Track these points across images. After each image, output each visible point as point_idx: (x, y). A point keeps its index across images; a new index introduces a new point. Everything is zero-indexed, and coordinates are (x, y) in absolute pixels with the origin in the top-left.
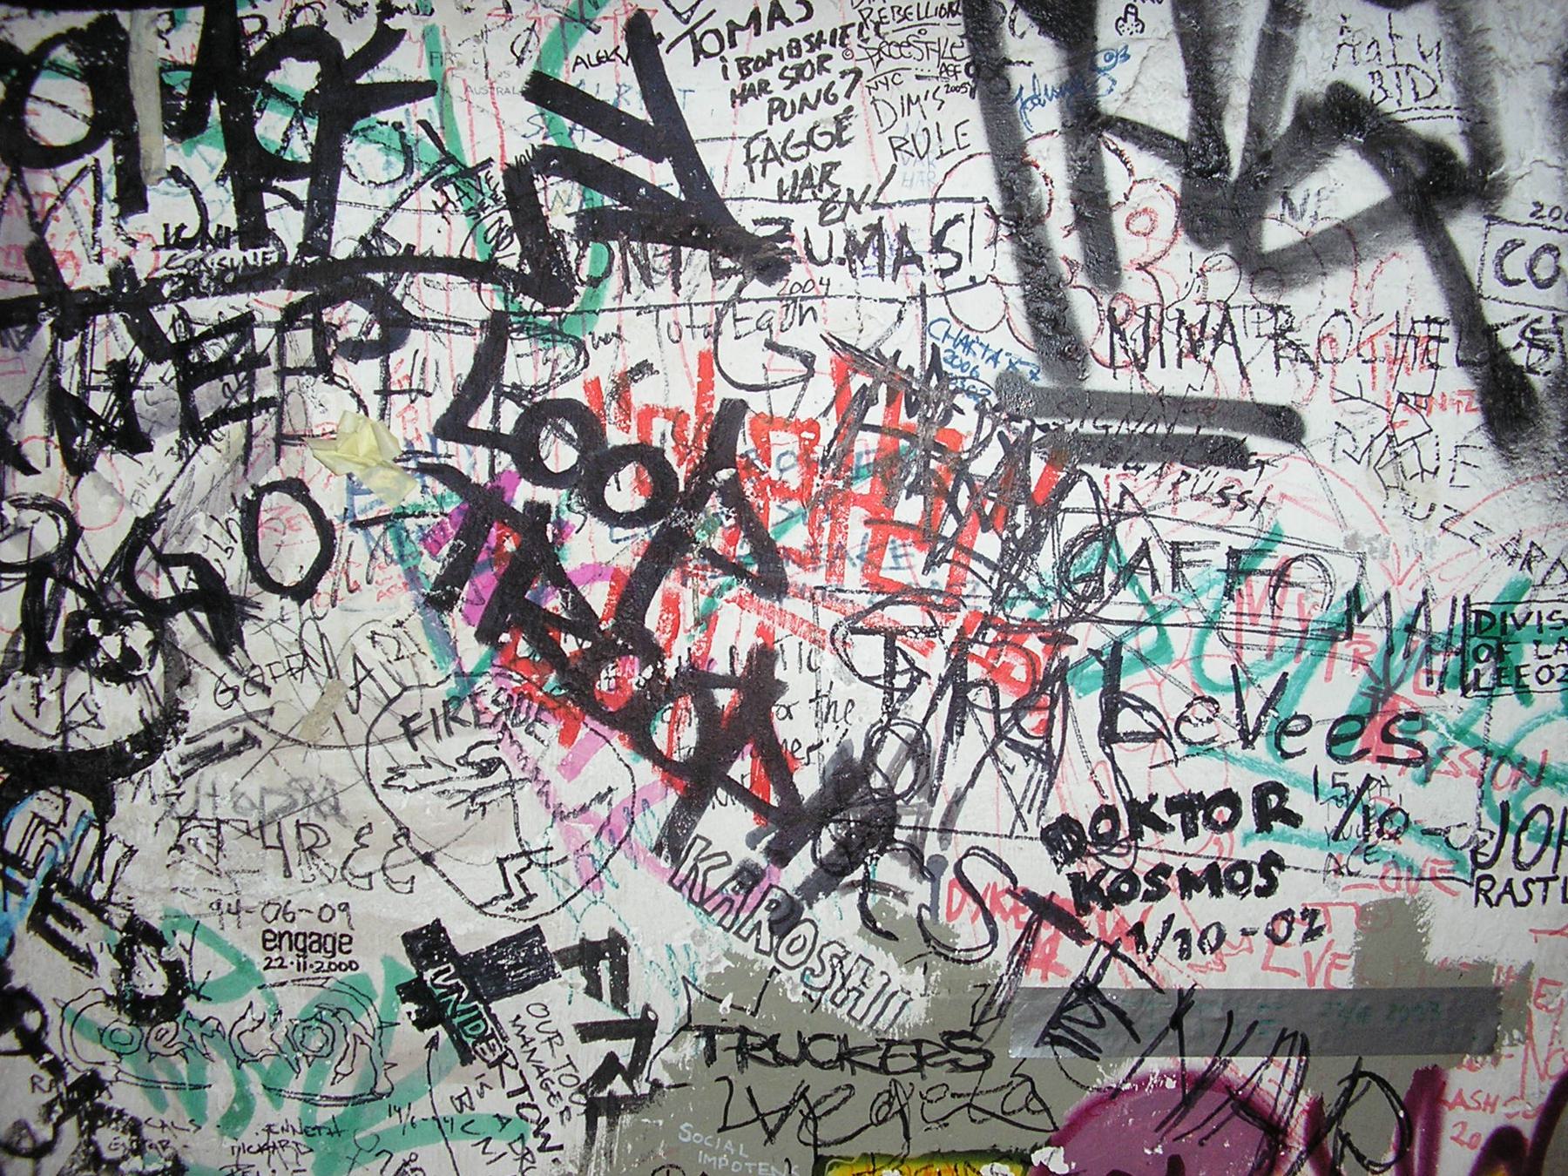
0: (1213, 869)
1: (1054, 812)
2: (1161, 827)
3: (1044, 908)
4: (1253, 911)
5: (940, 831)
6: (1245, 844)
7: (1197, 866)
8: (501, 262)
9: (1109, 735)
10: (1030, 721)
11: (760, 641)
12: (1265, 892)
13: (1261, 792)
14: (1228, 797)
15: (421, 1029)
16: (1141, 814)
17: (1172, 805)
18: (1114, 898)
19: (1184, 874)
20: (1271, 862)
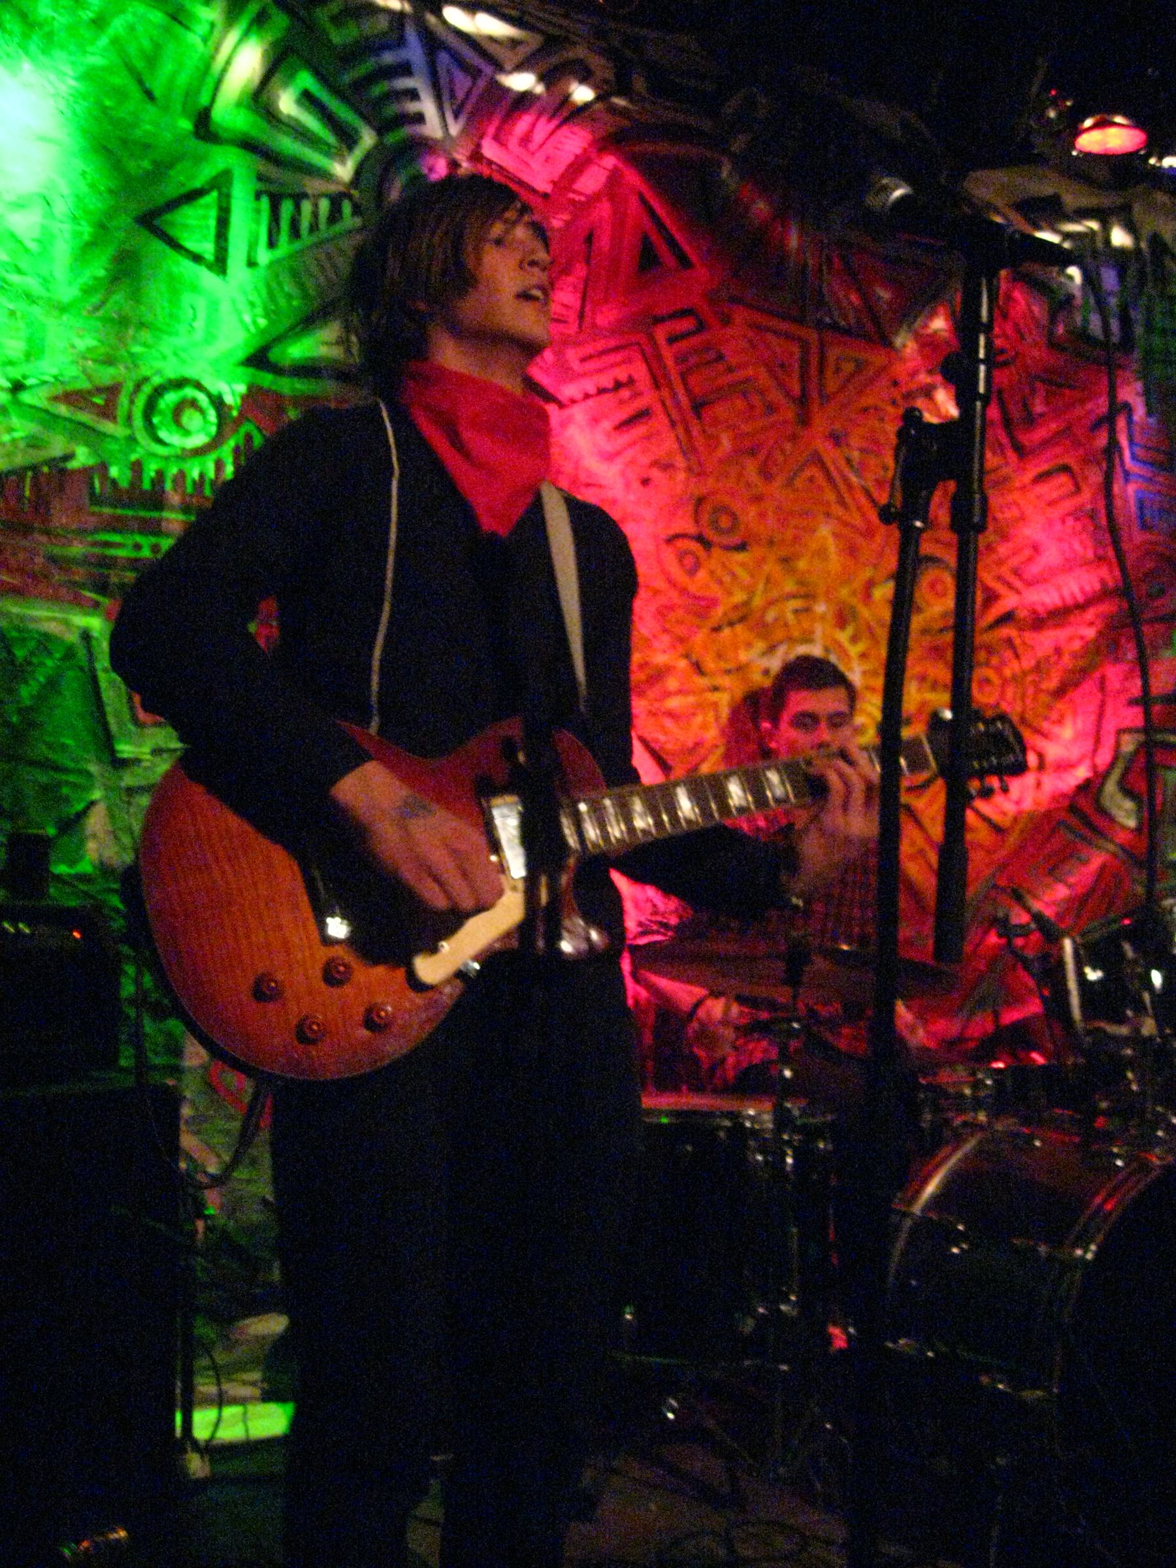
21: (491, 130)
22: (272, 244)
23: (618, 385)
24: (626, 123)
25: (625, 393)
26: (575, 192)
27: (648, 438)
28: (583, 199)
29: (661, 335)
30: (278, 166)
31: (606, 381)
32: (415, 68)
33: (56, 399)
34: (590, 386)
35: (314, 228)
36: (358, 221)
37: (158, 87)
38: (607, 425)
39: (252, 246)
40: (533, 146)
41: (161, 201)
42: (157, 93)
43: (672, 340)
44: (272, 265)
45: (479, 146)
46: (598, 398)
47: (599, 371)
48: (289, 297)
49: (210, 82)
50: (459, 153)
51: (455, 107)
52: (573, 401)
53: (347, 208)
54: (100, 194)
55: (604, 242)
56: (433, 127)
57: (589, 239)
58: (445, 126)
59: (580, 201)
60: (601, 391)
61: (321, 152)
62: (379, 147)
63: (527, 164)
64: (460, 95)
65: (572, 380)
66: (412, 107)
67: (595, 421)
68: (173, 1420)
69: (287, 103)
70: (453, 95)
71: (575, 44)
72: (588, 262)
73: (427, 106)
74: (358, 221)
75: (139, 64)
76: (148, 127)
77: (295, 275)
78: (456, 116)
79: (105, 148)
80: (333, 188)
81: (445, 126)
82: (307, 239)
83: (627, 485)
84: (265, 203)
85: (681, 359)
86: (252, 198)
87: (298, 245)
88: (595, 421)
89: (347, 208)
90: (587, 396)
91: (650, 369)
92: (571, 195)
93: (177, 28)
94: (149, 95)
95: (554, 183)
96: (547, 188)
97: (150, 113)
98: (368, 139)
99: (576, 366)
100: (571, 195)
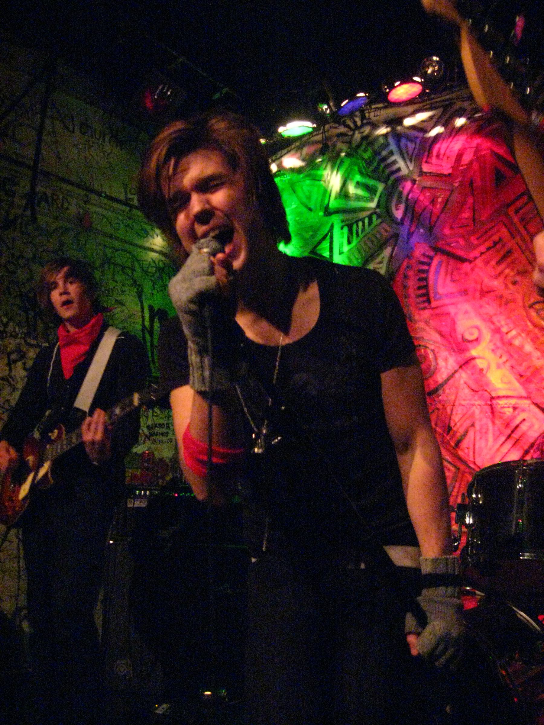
0: (162, 433)
1: (148, 424)
2: (157, 427)
3: (146, 436)
4: (164, 438)
5: (491, 317)
6: (164, 430)
7: (161, 432)
8: (171, 196)
9: (153, 416)
10: (146, 413)
11: (306, 221)
12: (167, 436)
13: (167, 424)
14: (163, 424)
15: (395, 160)
16: (156, 425)
17: (159, 424)
18: (153, 436)
19: (160, 433)
20: (167, 433)
21: (424, 160)
22: (349, 242)
23: (495, 244)
24: (480, 123)
25: (499, 246)
26: (462, 166)
27: (513, 263)
28: (465, 167)
29: (511, 211)
30: (355, 213)
31: (488, 244)
32: (394, 152)
33: (118, 337)
34: (482, 249)
35: (363, 230)
36: (380, 221)
37: (312, 205)
38: (493, 263)
39: (341, 246)
40: (441, 156)
41: (315, 243)
42: (312, 207)
43: (517, 212)
44: (350, 250)
45: (421, 169)
46: (488, 253)
47: (486, 241)
48: (358, 259)
49: (327, 195)
50: (414, 176)
51: (409, 158)
52: (475, 258)
53: (374, 217)
54: (298, 249)
55: (478, 182)
56: (405, 171)
57: (471, 182)
58: (408, 167)
59: (464, 169)
60: (489, 249)
61: (365, 201)
62: (385, 188)
63: (441, 166)
64: (410, 153)
65: (474, 249)
66: (397, 166)
67: (487, 263)
68: (520, 621)
69: (352, 189)
70: (408, 154)
71: (455, 103)
72: (473, 195)
73: (401, 164)
74: (380, 221)
75: (305, 200)
76: (311, 220)
77: (359, 252)
78: (411, 161)
79: (298, 234)
80: (369, 213)
81: (408, 167)
82: (361, 236)
83: (506, 287)
84: (346, 229)
85: (522, 220)
86: (340, 229)
87: (359, 239)
88: (487, 263)
89: (374, 217)
90: (482, 254)
91: (509, 230)
92: (461, 168)
93: (317, 183)
94: (310, 209)
95: (452, 167)
96: (450, 171)
97: (312, 214)
98: (381, 187)
99: (475, 242)
100: (461, 168)
